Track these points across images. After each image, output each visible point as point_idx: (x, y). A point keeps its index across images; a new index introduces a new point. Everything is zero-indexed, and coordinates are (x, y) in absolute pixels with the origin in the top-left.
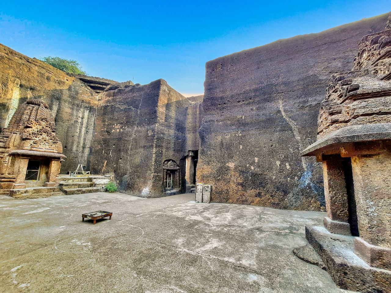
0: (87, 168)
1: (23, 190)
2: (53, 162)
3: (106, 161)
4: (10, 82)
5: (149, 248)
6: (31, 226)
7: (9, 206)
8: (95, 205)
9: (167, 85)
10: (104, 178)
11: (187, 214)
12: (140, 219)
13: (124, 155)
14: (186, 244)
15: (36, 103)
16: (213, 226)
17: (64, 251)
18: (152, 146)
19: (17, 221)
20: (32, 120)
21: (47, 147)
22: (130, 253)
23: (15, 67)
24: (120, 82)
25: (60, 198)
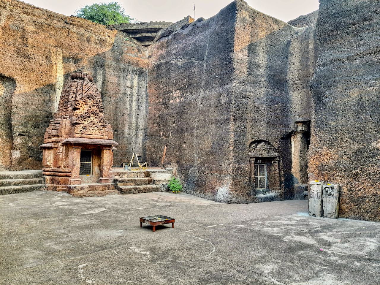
0: (142, 158)
1: (78, 186)
2: (105, 151)
3: (166, 147)
4: (53, 55)
5: (221, 269)
6: (90, 227)
7: (68, 204)
8: (154, 208)
9: (247, 9)
10: (165, 172)
11: (288, 232)
12: (211, 231)
13: (188, 137)
14: (276, 273)
15: (80, 77)
16: (332, 255)
17: (124, 257)
18: (228, 119)
19: (77, 221)
20: (79, 100)
21: (97, 132)
22: (195, 271)
23: (55, 34)
24: (174, 22)
25: (115, 198)
